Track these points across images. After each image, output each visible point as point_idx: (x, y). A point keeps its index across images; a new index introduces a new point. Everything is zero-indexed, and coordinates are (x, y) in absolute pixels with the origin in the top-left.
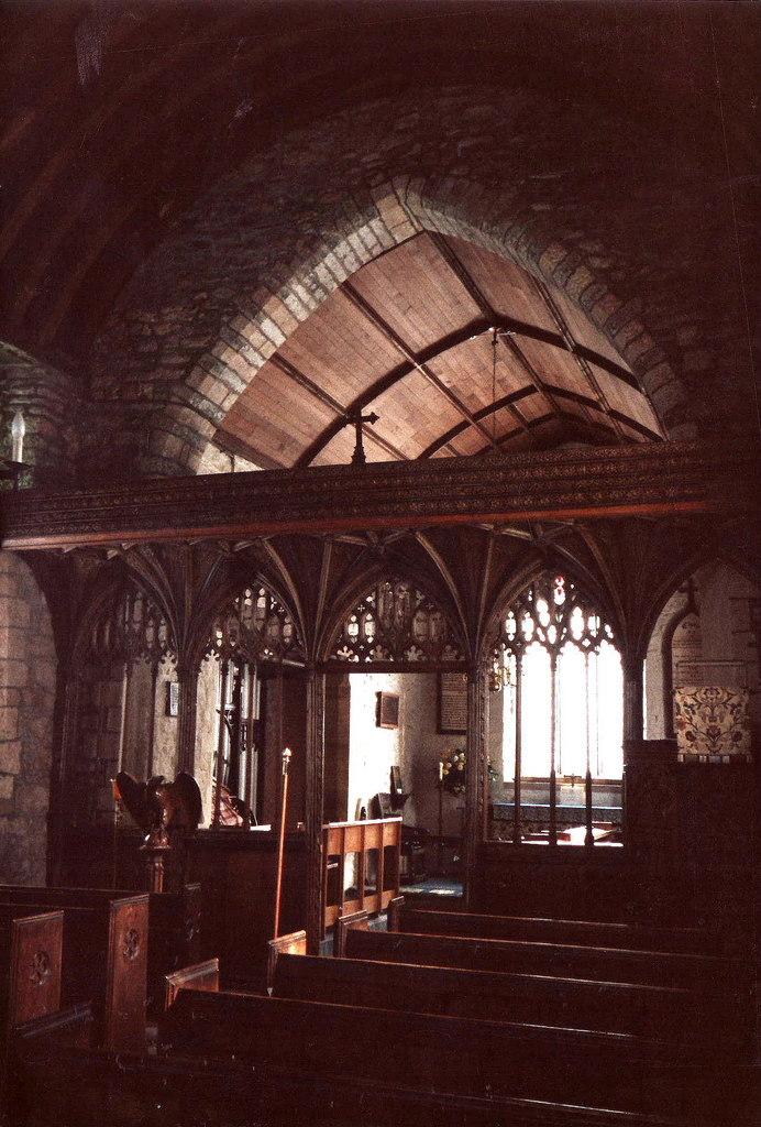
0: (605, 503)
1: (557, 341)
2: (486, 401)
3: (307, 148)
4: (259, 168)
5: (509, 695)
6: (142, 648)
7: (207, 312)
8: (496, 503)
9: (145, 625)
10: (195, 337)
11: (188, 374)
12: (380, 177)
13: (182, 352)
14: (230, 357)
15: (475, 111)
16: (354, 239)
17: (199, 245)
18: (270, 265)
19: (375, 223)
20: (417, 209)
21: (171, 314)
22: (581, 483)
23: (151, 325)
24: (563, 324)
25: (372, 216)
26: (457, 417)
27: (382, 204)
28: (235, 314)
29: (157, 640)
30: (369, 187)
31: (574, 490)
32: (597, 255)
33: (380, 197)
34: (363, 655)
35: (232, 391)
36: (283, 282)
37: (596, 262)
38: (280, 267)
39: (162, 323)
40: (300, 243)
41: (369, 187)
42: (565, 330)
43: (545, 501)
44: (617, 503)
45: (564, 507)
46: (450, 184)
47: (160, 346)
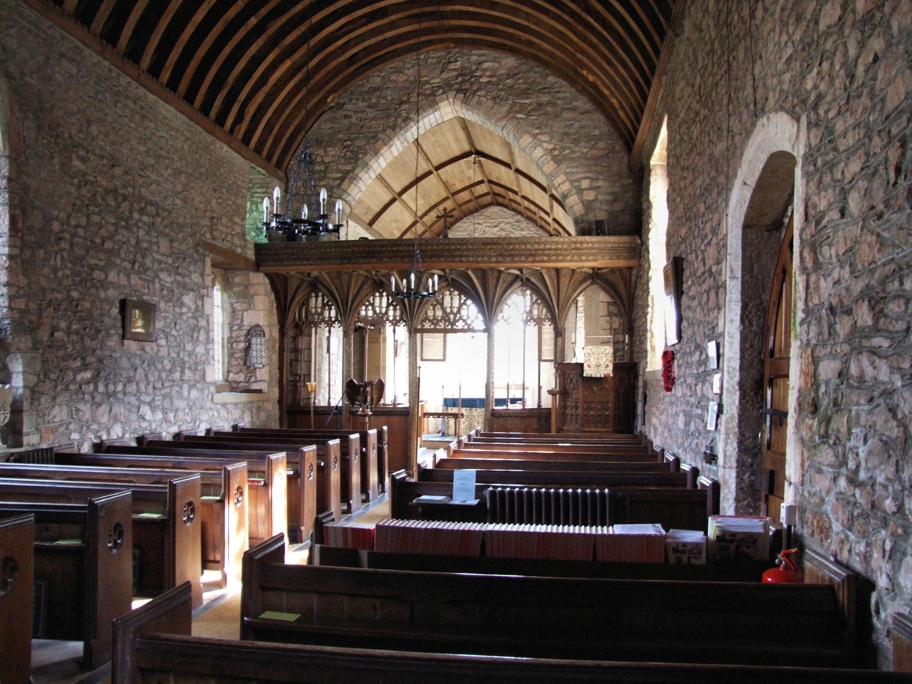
0: (557, 261)
1: (508, 165)
2: (459, 186)
3: (402, 73)
4: (378, 80)
5: (325, 367)
6: (323, 320)
7: (351, 151)
8: (509, 259)
9: (323, 308)
10: (345, 164)
11: (342, 182)
12: (441, 91)
13: (338, 171)
14: (363, 175)
15: (486, 65)
16: (426, 120)
17: (346, 116)
18: (384, 130)
19: (437, 113)
20: (458, 108)
21: (332, 151)
22: (546, 252)
23: (321, 156)
24: (511, 154)
25: (436, 110)
26: (444, 194)
27: (441, 105)
28: (365, 154)
29: (395, 316)
30: (435, 96)
31: (543, 255)
32: (546, 142)
33: (442, 101)
34: (435, 324)
35: (361, 191)
36: (390, 139)
37: (545, 145)
38: (389, 131)
39: (326, 155)
40: (400, 120)
41: (435, 96)
42: (513, 160)
43: (530, 259)
44: (560, 261)
45: (539, 262)
46: (476, 99)
47: (327, 168)
